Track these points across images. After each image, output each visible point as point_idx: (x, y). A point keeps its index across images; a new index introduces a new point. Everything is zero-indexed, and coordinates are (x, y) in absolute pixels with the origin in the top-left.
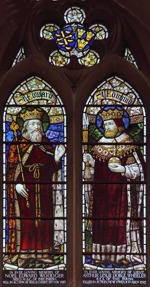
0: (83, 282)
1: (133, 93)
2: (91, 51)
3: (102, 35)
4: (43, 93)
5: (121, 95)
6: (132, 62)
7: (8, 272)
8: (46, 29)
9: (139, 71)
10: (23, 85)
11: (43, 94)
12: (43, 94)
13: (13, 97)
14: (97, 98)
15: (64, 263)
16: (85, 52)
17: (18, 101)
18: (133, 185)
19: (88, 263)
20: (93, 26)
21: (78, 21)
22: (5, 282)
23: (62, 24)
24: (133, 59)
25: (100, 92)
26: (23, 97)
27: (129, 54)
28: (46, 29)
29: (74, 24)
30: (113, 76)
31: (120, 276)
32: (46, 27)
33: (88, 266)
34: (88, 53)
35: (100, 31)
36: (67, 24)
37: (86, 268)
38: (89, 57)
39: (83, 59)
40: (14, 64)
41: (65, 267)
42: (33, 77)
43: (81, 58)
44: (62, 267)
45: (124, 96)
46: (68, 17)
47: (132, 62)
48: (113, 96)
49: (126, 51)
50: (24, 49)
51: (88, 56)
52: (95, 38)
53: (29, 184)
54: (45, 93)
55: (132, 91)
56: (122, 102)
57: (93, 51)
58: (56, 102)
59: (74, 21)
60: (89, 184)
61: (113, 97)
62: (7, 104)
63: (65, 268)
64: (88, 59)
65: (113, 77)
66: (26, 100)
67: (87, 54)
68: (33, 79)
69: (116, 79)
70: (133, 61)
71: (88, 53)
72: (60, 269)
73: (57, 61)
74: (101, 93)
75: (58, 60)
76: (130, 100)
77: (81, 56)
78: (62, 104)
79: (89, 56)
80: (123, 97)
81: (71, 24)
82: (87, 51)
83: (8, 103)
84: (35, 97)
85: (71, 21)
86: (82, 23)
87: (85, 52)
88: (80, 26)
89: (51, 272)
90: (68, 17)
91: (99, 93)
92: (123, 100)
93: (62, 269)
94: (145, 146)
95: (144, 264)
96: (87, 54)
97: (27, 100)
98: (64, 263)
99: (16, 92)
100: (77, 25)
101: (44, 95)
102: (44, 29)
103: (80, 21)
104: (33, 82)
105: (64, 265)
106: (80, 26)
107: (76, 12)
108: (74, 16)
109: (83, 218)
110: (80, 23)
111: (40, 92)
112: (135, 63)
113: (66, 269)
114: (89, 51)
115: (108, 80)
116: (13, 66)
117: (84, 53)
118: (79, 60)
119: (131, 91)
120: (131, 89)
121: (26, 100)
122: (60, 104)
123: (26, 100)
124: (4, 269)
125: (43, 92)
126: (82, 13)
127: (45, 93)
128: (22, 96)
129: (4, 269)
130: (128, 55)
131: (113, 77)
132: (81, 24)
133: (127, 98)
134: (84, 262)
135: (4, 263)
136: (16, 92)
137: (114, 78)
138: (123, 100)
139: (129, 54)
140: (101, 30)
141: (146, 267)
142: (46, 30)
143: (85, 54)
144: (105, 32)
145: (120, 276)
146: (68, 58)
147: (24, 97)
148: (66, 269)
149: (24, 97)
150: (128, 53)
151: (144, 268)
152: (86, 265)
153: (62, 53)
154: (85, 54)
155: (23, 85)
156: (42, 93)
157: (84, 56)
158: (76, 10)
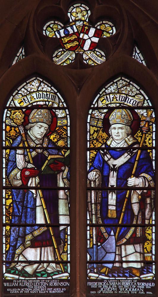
0: (8, 290)
1: (141, 94)
6: (141, 62)
9: (147, 68)
13: (12, 100)
15: (152, 273)
19: (9, 272)
20: (99, 24)
21: (83, 19)
22: (92, 292)
23: (66, 22)
24: (142, 59)
25: (104, 97)
27: (22, 54)
30: (35, 77)
31: (56, 284)
33: (9, 276)
36: (72, 22)
37: (91, 278)
40: (14, 63)
41: (68, 276)
42: (34, 78)
44: (150, 276)
48: (40, 97)
49: (20, 51)
53: (48, 189)
55: (140, 92)
56: (125, 103)
58: (144, 103)
62: (92, 106)
63: (153, 278)
68: (35, 80)
70: (142, 61)
76: (38, 95)
78: (150, 105)
84: (41, 98)
89: (131, 281)
91: (103, 98)
95: (68, 273)
97: (29, 102)
98: (152, 273)
104: (36, 84)
105: (67, 274)
107: (80, 10)
108: (78, 15)
110: (85, 21)
111: (125, 96)
112: (143, 62)
113: (69, 278)
115: (115, 81)
116: (13, 65)
119: (138, 92)
120: (139, 90)
121: (28, 101)
123: (109, 100)
124: (88, 278)
129: (88, 278)
130: (136, 54)
134: (4, 272)
135: (89, 271)
137: (36, 79)
138: (127, 101)
139: (22, 54)
141: (70, 276)
145: (56, 284)
148: (69, 278)
151: (68, 278)
152: (6, 275)
158: (87, 15)
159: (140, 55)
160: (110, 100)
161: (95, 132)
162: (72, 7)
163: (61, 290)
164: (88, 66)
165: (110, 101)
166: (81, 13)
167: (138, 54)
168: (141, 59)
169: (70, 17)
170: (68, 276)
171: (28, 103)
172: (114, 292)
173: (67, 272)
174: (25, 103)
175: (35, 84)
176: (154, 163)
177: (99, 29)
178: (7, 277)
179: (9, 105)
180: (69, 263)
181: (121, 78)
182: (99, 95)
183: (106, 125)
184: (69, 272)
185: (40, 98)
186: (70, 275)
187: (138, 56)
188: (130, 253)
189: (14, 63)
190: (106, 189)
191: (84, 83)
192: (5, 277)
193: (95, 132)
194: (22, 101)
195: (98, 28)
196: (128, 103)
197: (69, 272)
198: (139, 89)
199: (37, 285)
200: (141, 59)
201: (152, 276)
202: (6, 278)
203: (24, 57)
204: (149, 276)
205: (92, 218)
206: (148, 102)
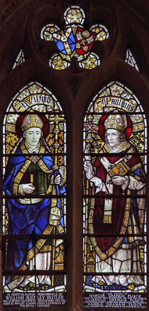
1: (134, 99)
2: (92, 53)
3: (102, 36)
4: (113, 100)
5: (46, 102)
6: (133, 66)
7: (87, 294)
8: (46, 30)
9: (140, 73)
10: (22, 92)
11: (113, 101)
12: (113, 101)
13: (12, 105)
14: (98, 106)
16: (86, 55)
17: (18, 109)
18: (116, 199)
20: (94, 26)
24: (135, 63)
25: (100, 100)
26: (102, 99)
28: (46, 30)
29: (74, 25)
30: (33, 81)
32: (47, 28)
34: (89, 55)
35: (100, 31)
36: (68, 25)
38: (89, 60)
39: (84, 62)
40: (14, 67)
43: (81, 61)
45: (126, 102)
46: (68, 17)
47: (133, 66)
50: (130, 50)
51: (88, 59)
52: (96, 40)
54: (114, 100)
56: (124, 108)
57: (94, 54)
59: (74, 21)
60: (59, 198)
61: (48, 103)
63: (65, 290)
64: (88, 62)
65: (33, 83)
66: (104, 103)
67: (87, 57)
68: (113, 84)
69: (36, 84)
70: (134, 64)
71: (89, 55)
72: (140, 291)
73: (91, 66)
74: (101, 100)
75: (90, 65)
77: (81, 59)
78: (143, 111)
79: (89, 59)
80: (125, 103)
81: (71, 24)
82: (87, 54)
83: (88, 111)
85: (70, 22)
86: (82, 23)
87: (85, 55)
88: (80, 26)
90: (68, 17)
92: (124, 106)
93: (142, 291)
94: (146, 156)
95: (145, 286)
96: (87, 57)
99: (15, 100)
100: (77, 26)
101: (114, 102)
102: (45, 31)
103: (79, 21)
105: (63, 287)
106: (80, 26)
109: (84, 236)
110: (80, 24)
114: (90, 54)
117: (84, 56)
118: (80, 64)
122: (141, 110)
123: (104, 103)
124: (3, 292)
125: (113, 99)
126: (81, 13)
127: (114, 100)
128: (21, 103)
129: (84, 291)
130: (130, 57)
131: (113, 82)
132: (81, 25)
133: (128, 104)
135: (84, 284)
136: (15, 100)
137: (115, 83)
138: (124, 106)
140: (102, 31)
141: (146, 289)
142: (47, 31)
143: (85, 58)
144: (106, 33)
146: (68, 61)
147: (103, 99)
148: (146, 291)
149: (103, 99)
150: (129, 55)
151: (145, 291)
153: (62, 56)
154: (85, 58)
155: (22, 92)
156: (112, 100)
157: (85, 59)
159: (133, 58)
160: (105, 104)
161: (51, 139)
162: (69, 8)
163: (26, 302)
164: (83, 70)
165: (105, 105)
166: (76, 15)
167: (131, 57)
168: (133, 63)
169: (66, 20)
170: (145, 290)
171: (27, 107)
172: (90, 306)
173: (63, 284)
174: (23, 107)
175: (35, 89)
176: (4, 169)
177: (93, 32)
178: (86, 289)
179: (9, 111)
180: (146, 275)
181: (115, 82)
182: (56, 100)
183: (102, 132)
184: (146, 286)
185: (48, 103)
186: (66, 288)
187: (131, 61)
188: (122, 265)
189: (14, 67)
190: (116, 197)
191: (80, 86)
192: (85, 289)
193: (51, 139)
194: (21, 107)
195: (93, 31)
196: (125, 108)
197: (146, 286)
198: (51, 94)
199: (60, 298)
200: (133, 63)
201: (63, 288)
202: (85, 290)
203: (24, 61)
204: (61, 288)
205: (88, 226)
206: (140, 109)
